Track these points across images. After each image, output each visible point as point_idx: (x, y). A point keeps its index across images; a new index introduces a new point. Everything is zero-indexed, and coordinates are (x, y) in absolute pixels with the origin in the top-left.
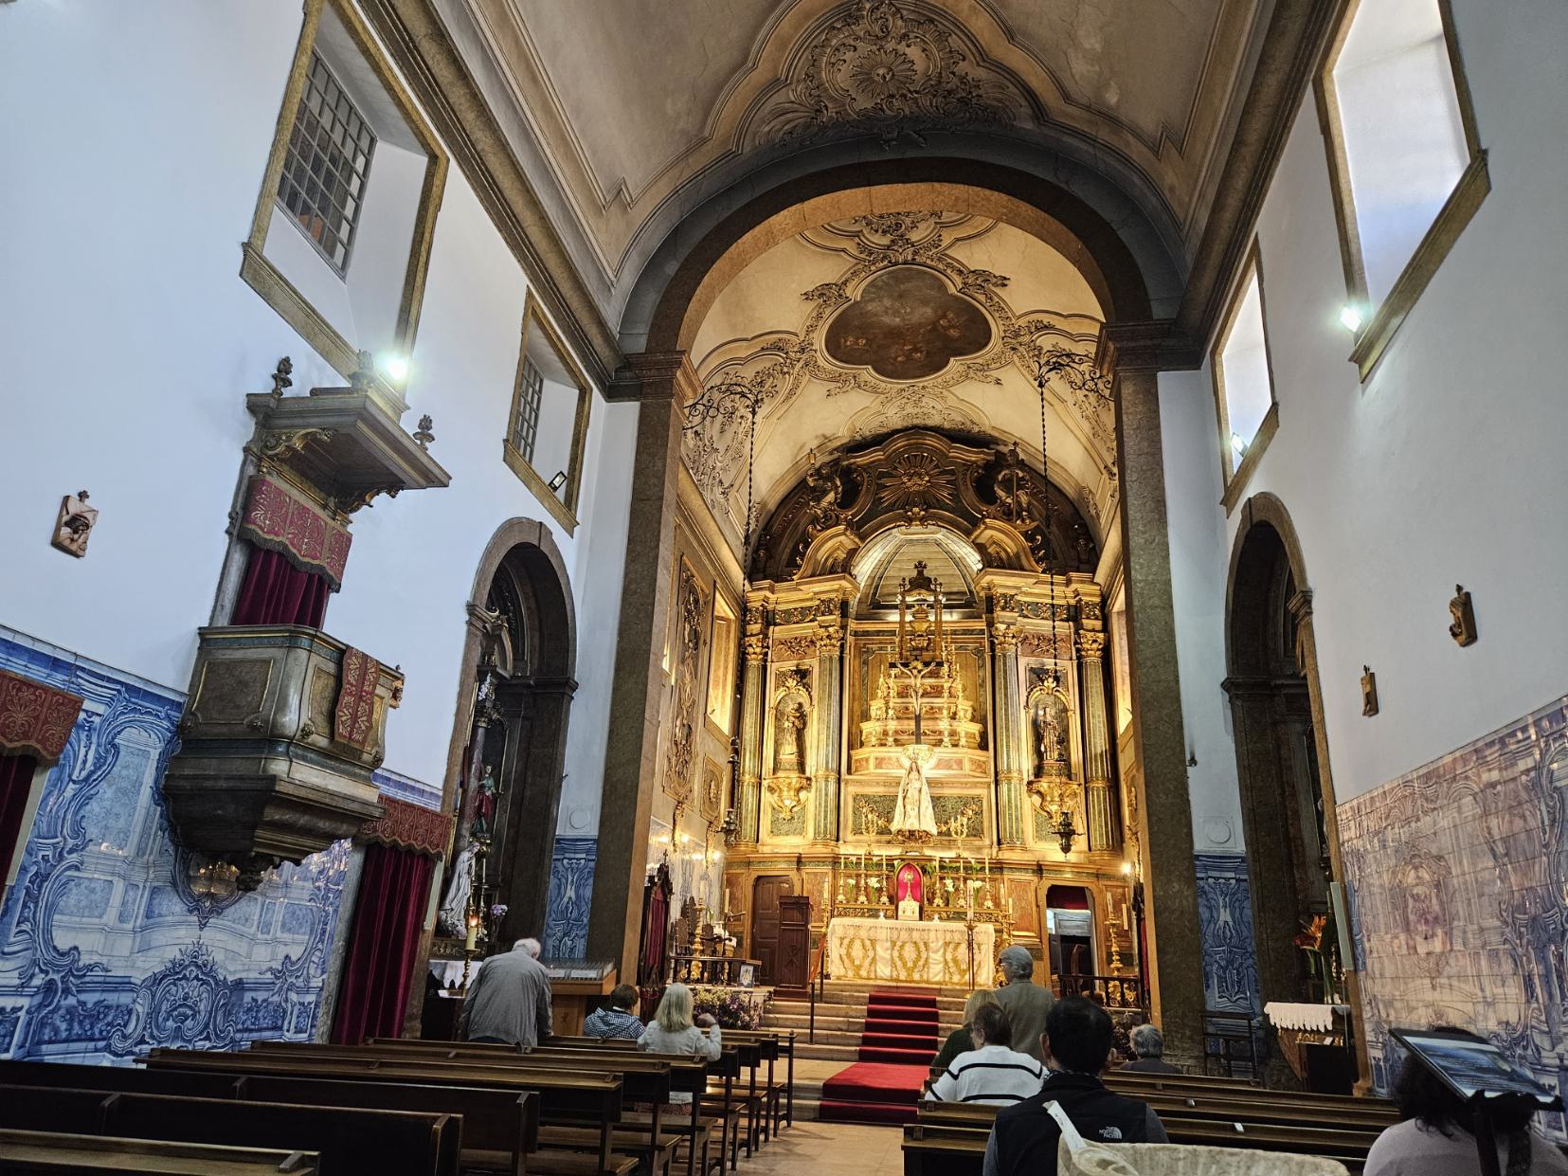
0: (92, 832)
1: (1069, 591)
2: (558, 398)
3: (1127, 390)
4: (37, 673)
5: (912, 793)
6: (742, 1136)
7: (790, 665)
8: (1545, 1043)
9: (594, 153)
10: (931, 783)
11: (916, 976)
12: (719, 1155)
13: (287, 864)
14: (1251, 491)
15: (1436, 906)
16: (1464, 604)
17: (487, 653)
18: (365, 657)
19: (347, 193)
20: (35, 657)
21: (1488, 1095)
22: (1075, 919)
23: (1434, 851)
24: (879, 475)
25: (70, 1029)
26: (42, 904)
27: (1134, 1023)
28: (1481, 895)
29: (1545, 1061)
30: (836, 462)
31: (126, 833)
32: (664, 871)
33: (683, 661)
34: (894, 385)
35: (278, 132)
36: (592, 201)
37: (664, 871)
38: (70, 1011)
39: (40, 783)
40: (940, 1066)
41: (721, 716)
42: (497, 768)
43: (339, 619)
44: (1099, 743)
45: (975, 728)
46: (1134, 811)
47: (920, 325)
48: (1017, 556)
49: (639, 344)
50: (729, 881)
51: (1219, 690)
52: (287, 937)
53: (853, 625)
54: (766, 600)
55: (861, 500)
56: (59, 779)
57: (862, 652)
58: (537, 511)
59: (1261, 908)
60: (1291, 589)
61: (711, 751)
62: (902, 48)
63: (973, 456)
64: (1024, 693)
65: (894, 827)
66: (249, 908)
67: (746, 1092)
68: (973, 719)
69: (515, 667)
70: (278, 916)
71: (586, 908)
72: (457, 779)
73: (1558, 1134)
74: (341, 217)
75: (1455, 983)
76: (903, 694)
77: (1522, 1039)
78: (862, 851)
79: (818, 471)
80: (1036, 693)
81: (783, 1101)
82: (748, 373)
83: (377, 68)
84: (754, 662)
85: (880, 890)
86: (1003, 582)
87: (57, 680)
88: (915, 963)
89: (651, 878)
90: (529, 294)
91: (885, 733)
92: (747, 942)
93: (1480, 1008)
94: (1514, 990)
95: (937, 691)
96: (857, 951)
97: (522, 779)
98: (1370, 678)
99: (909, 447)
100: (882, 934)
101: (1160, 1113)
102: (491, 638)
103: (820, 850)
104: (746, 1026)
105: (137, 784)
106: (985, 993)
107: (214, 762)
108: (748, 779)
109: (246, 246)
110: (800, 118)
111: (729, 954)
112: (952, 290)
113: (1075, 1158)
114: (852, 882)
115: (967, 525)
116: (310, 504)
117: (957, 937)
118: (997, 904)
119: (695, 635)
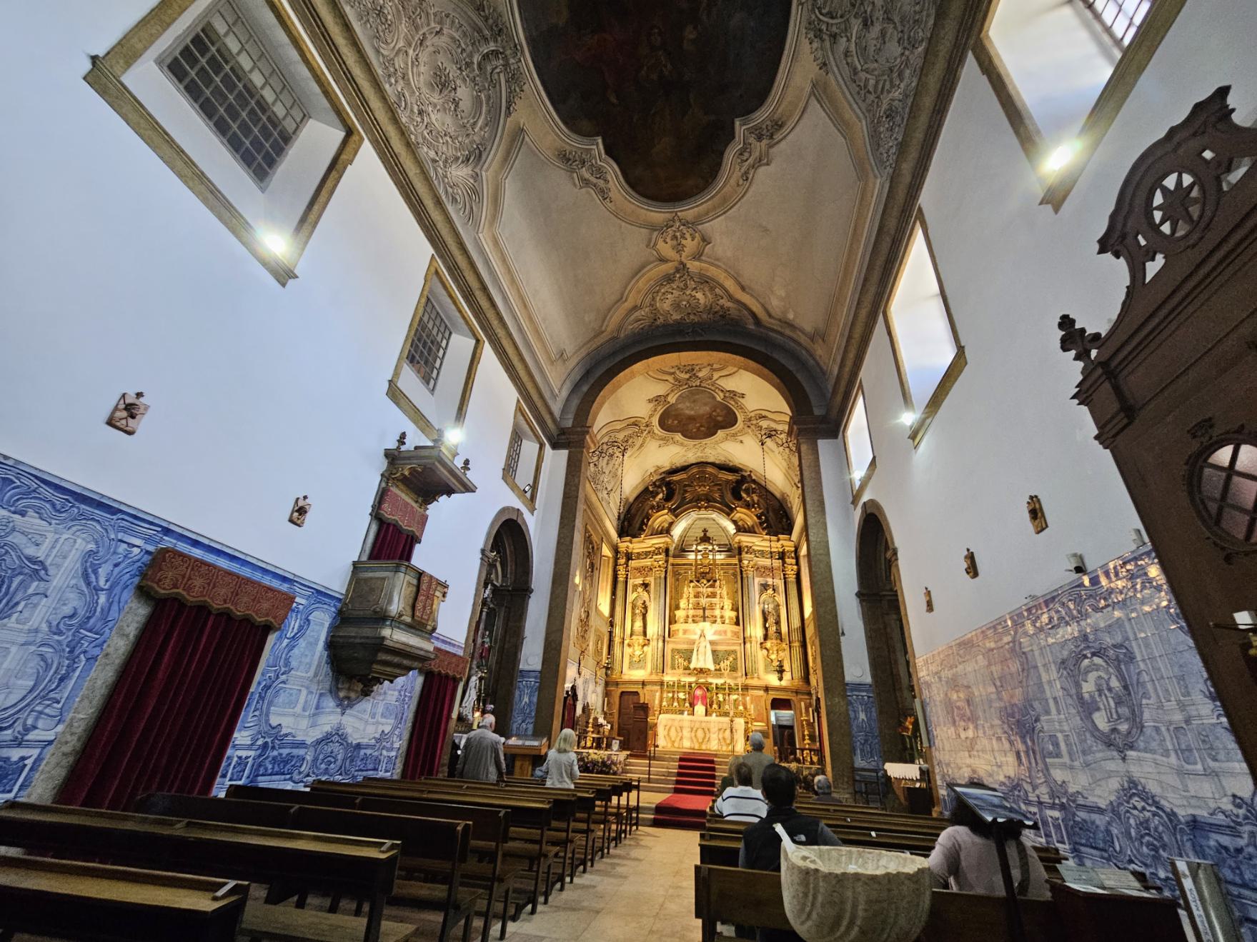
0: (294, 664)
1: (779, 545)
2: (529, 448)
3: (804, 448)
4: (275, 584)
5: (701, 649)
6: (613, 835)
7: (640, 581)
8: (1028, 788)
9: (551, 338)
10: (712, 643)
11: (704, 747)
12: (583, 857)
13: (386, 683)
14: (865, 498)
15: (968, 713)
16: (971, 557)
17: (489, 574)
18: (431, 577)
19: (437, 356)
20: (275, 575)
21: (1000, 820)
22: (786, 715)
23: (966, 684)
24: (684, 486)
25: (273, 768)
26: (266, 702)
27: (817, 774)
28: (991, 707)
29: (1030, 799)
30: (663, 479)
31: (310, 664)
32: (574, 688)
33: (586, 578)
34: (691, 443)
35: (409, 331)
36: (549, 358)
37: (574, 688)
38: (274, 758)
39: (272, 638)
40: (715, 795)
41: (605, 608)
42: (491, 633)
43: (421, 557)
44: (796, 623)
45: (733, 614)
46: (815, 659)
47: (703, 415)
48: (753, 526)
49: (569, 423)
50: (607, 694)
51: (855, 597)
52: (384, 720)
53: (671, 560)
54: (627, 547)
55: (675, 498)
56: (281, 637)
57: (676, 574)
58: (516, 503)
59: (881, 712)
60: (887, 548)
61: (601, 626)
62: (694, 293)
63: (731, 477)
64: (757, 596)
65: (692, 666)
66: (366, 705)
67: (615, 810)
68: (732, 609)
69: (503, 581)
70: (380, 709)
71: (534, 707)
72: (471, 639)
73: (1040, 839)
74: (434, 367)
75: (980, 754)
76: (697, 596)
77: (1016, 786)
78: (675, 679)
79: (654, 483)
80: (764, 596)
81: (634, 815)
82: (621, 436)
83: (455, 302)
84: (621, 579)
85: (685, 700)
86: (746, 539)
87: (284, 587)
88: (704, 739)
89: (567, 692)
90: (518, 401)
91: (688, 617)
92: (616, 726)
93: (995, 768)
94: (1011, 759)
95: (713, 595)
96: (673, 733)
97: (504, 637)
98: (928, 593)
99: (698, 473)
100: (686, 724)
101: (829, 826)
102: (492, 566)
103: (654, 678)
104: (615, 773)
105: (317, 640)
106: (737, 757)
107: (355, 629)
108: (617, 640)
109: (390, 382)
110: (647, 323)
111: (607, 733)
112: (719, 399)
113: (790, 855)
114: (670, 695)
115: (728, 511)
116: (410, 501)
117: (725, 726)
118: (745, 708)
119: (592, 565)
